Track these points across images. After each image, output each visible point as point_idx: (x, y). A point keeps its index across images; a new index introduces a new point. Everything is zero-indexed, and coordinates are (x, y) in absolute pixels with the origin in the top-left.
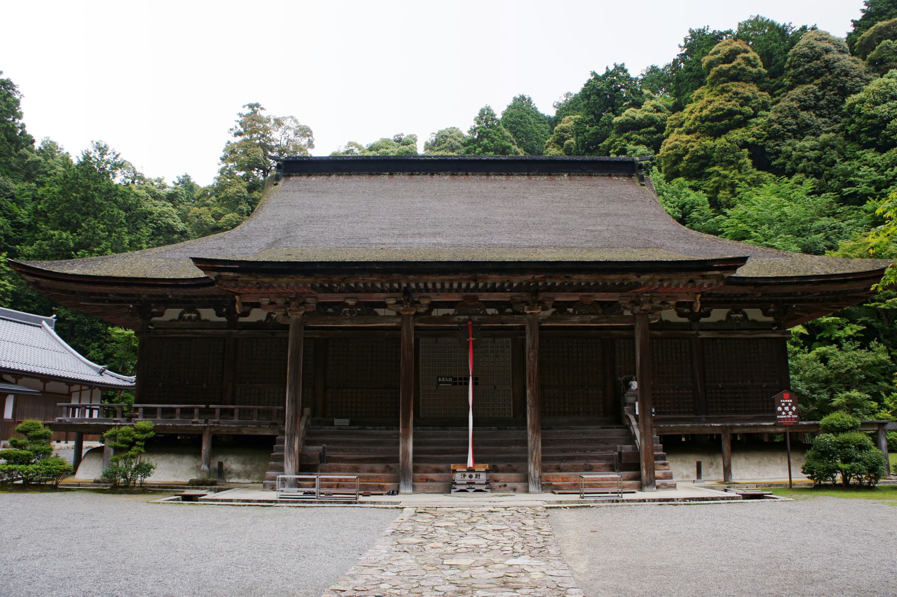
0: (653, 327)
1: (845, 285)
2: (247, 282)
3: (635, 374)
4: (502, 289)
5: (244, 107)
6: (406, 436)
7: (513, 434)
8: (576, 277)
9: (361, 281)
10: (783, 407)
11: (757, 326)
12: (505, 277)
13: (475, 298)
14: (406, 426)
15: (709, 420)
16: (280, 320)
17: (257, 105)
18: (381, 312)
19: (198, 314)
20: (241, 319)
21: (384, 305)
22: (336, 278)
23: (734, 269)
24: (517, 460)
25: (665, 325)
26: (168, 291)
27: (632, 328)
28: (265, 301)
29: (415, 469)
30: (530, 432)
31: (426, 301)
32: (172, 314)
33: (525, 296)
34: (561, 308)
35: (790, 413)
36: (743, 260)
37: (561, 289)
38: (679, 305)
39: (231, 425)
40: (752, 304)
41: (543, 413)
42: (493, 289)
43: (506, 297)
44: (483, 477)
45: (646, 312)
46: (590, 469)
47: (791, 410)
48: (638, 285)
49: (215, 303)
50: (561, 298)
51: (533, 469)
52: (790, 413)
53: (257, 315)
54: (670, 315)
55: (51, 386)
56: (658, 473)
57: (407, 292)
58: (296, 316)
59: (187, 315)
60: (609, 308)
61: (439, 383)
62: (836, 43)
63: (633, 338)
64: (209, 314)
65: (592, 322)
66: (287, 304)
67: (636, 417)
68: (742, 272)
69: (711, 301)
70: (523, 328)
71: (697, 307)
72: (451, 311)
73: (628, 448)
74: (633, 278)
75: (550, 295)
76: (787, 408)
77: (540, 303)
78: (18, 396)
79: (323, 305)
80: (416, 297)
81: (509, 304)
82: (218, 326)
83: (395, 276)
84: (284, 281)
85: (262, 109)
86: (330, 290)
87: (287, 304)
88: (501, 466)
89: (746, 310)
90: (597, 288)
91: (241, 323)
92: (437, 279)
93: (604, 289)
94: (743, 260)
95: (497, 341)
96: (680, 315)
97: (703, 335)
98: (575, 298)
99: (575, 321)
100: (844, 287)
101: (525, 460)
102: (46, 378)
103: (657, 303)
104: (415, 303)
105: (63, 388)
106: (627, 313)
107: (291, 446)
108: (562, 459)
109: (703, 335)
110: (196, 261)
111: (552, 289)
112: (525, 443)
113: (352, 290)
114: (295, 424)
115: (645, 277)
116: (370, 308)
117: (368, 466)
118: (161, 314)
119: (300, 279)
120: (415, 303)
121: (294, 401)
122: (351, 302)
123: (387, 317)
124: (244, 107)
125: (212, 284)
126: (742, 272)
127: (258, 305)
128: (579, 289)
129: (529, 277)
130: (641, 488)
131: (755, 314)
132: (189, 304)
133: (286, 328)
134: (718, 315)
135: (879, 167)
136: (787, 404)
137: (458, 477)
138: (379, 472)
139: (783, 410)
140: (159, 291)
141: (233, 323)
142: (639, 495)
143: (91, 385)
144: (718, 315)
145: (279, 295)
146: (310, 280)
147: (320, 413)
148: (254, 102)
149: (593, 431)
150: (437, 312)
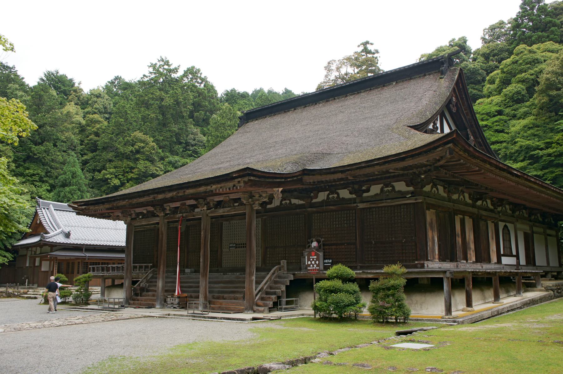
1: (405, 163)
5: (359, 46)
10: (311, 262)
11: (403, 195)
17: (367, 43)
19: (393, 187)
35: (315, 266)
40: (398, 178)
47: (315, 263)
52: (315, 266)
59: (386, 189)
61: (230, 247)
62: (22, 85)
65: (228, 212)
75: (212, 198)
76: (313, 262)
85: (372, 44)
89: (394, 184)
91: (269, 208)
95: (231, 222)
118: (368, 190)
124: (359, 46)
135: (221, 102)
136: (313, 259)
139: (311, 263)
148: (365, 41)
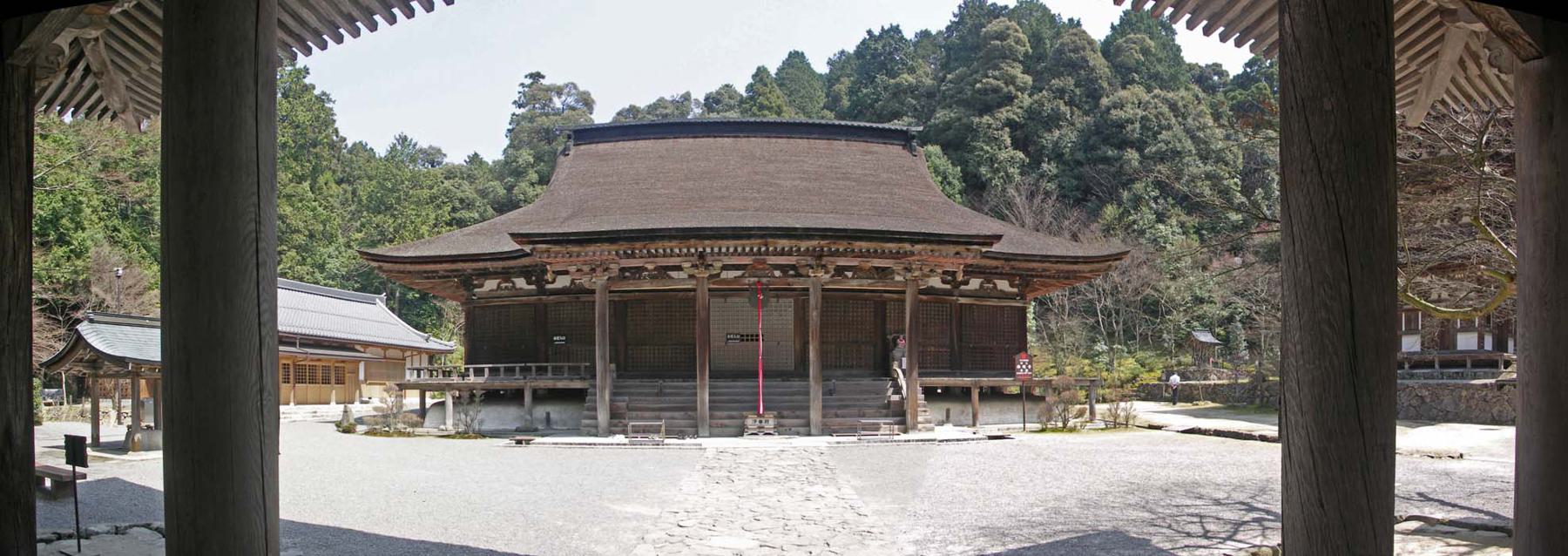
0: (921, 292)
2: (557, 253)
3: (903, 331)
4: (790, 254)
6: (703, 388)
7: (796, 384)
8: (858, 243)
9: (660, 246)
11: (1005, 296)
12: (794, 242)
13: (764, 262)
14: (702, 379)
15: (962, 375)
16: (587, 286)
18: (674, 274)
20: (549, 286)
21: (679, 268)
22: (638, 245)
23: (991, 244)
24: (798, 408)
25: (930, 291)
26: (488, 265)
27: (904, 292)
28: (573, 269)
29: (711, 417)
30: (812, 382)
31: (719, 264)
32: (491, 285)
33: (810, 260)
34: (840, 271)
36: (999, 237)
37: (844, 254)
38: (945, 273)
39: (546, 383)
40: (1002, 276)
41: (825, 365)
42: (782, 253)
43: (792, 260)
44: (772, 423)
45: (916, 279)
46: (863, 416)
48: (912, 254)
49: (526, 273)
50: (842, 262)
51: (815, 415)
53: (563, 282)
54: (935, 282)
55: (390, 353)
56: (920, 419)
57: (702, 256)
58: (599, 281)
60: (883, 273)
62: (1091, 42)
63: (903, 301)
64: (521, 283)
66: (593, 270)
67: (904, 372)
68: (996, 248)
69: (971, 271)
70: (807, 290)
71: (960, 277)
72: (739, 273)
73: (896, 398)
74: (907, 247)
77: (824, 266)
78: (368, 362)
79: (623, 270)
80: (709, 260)
81: (793, 267)
82: (529, 294)
83: (692, 241)
84: (591, 248)
86: (633, 256)
87: (593, 270)
88: (785, 413)
90: (876, 254)
92: (731, 243)
93: (883, 255)
94: (999, 237)
96: (944, 282)
97: (962, 300)
98: (855, 262)
99: (854, 284)
100: (1075, 267)
101: (808, 408)
102: (386, 347)
103: (926, 270)
104: (708, 266)
105: (398, 354)
106: (898, 278)
107: (603, 397)
108: (839, 407)
109: (962, 300)
110: (512, 235)
111: (836, 254)
112: (808, 394)
113: (650, 255)
114: (604, 379)
115: (918, 247)
116: (663, 271)
117: (668, 414)
118: (481, 286)
119: (606, 246)
120: (708, 266)
121: (603, 357)
122: (650, 267)
123: (680, 280)
125: (527, 255)
126: (996, 248)
127: (566, 273)
128: (861, 255)
129: (815, 243)
130: (905, 432)
131: (1003, 285)
132: (506, 275)
133: (593, 292)
134: (975, 284)
137: (749, 422)
138: (680, 420)
140: (481, 265)
141: (541, 291)
142: (903, 437)
143: (419, 350)
144: (975, 284)
145: (585, 263)
146: (614, 247)
147: (627, 367)
149: (867, 382)
150: (724, 275)
